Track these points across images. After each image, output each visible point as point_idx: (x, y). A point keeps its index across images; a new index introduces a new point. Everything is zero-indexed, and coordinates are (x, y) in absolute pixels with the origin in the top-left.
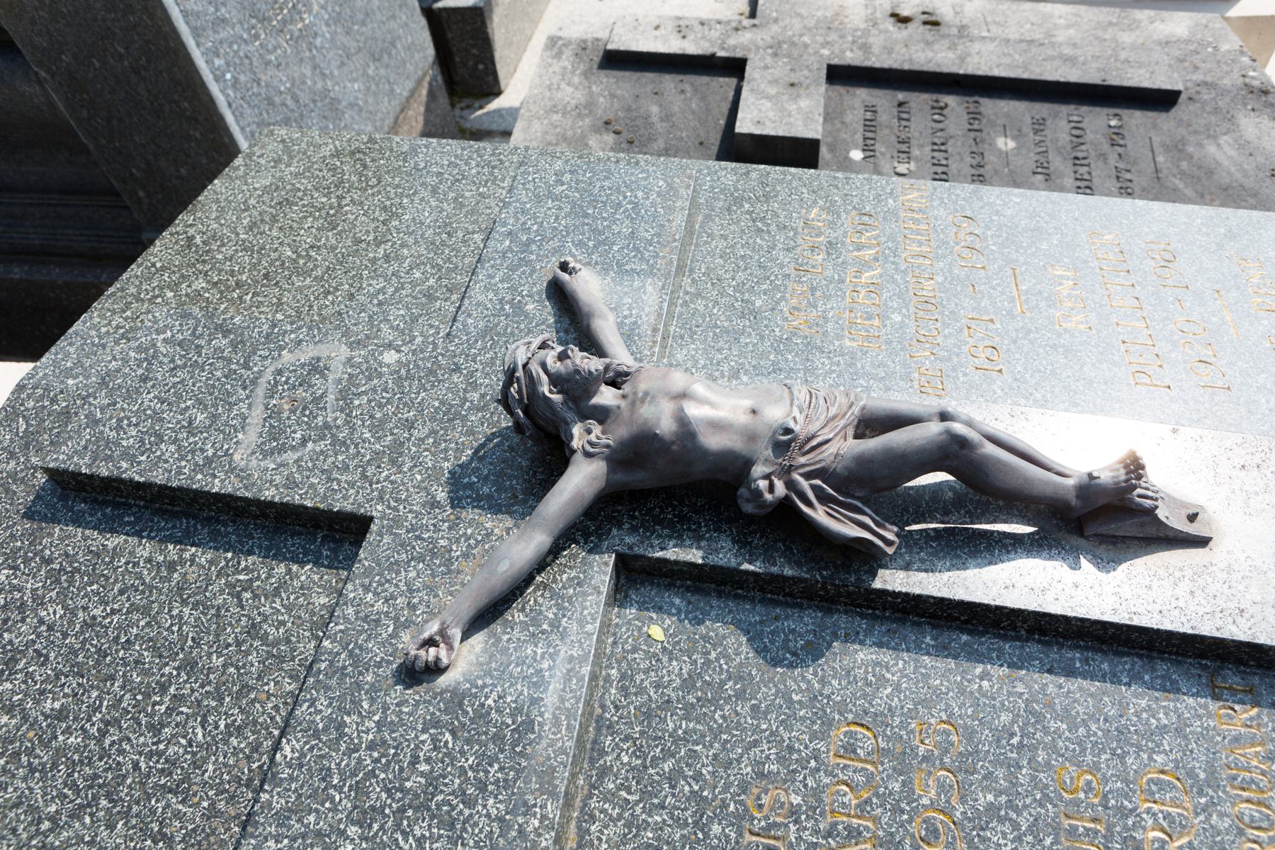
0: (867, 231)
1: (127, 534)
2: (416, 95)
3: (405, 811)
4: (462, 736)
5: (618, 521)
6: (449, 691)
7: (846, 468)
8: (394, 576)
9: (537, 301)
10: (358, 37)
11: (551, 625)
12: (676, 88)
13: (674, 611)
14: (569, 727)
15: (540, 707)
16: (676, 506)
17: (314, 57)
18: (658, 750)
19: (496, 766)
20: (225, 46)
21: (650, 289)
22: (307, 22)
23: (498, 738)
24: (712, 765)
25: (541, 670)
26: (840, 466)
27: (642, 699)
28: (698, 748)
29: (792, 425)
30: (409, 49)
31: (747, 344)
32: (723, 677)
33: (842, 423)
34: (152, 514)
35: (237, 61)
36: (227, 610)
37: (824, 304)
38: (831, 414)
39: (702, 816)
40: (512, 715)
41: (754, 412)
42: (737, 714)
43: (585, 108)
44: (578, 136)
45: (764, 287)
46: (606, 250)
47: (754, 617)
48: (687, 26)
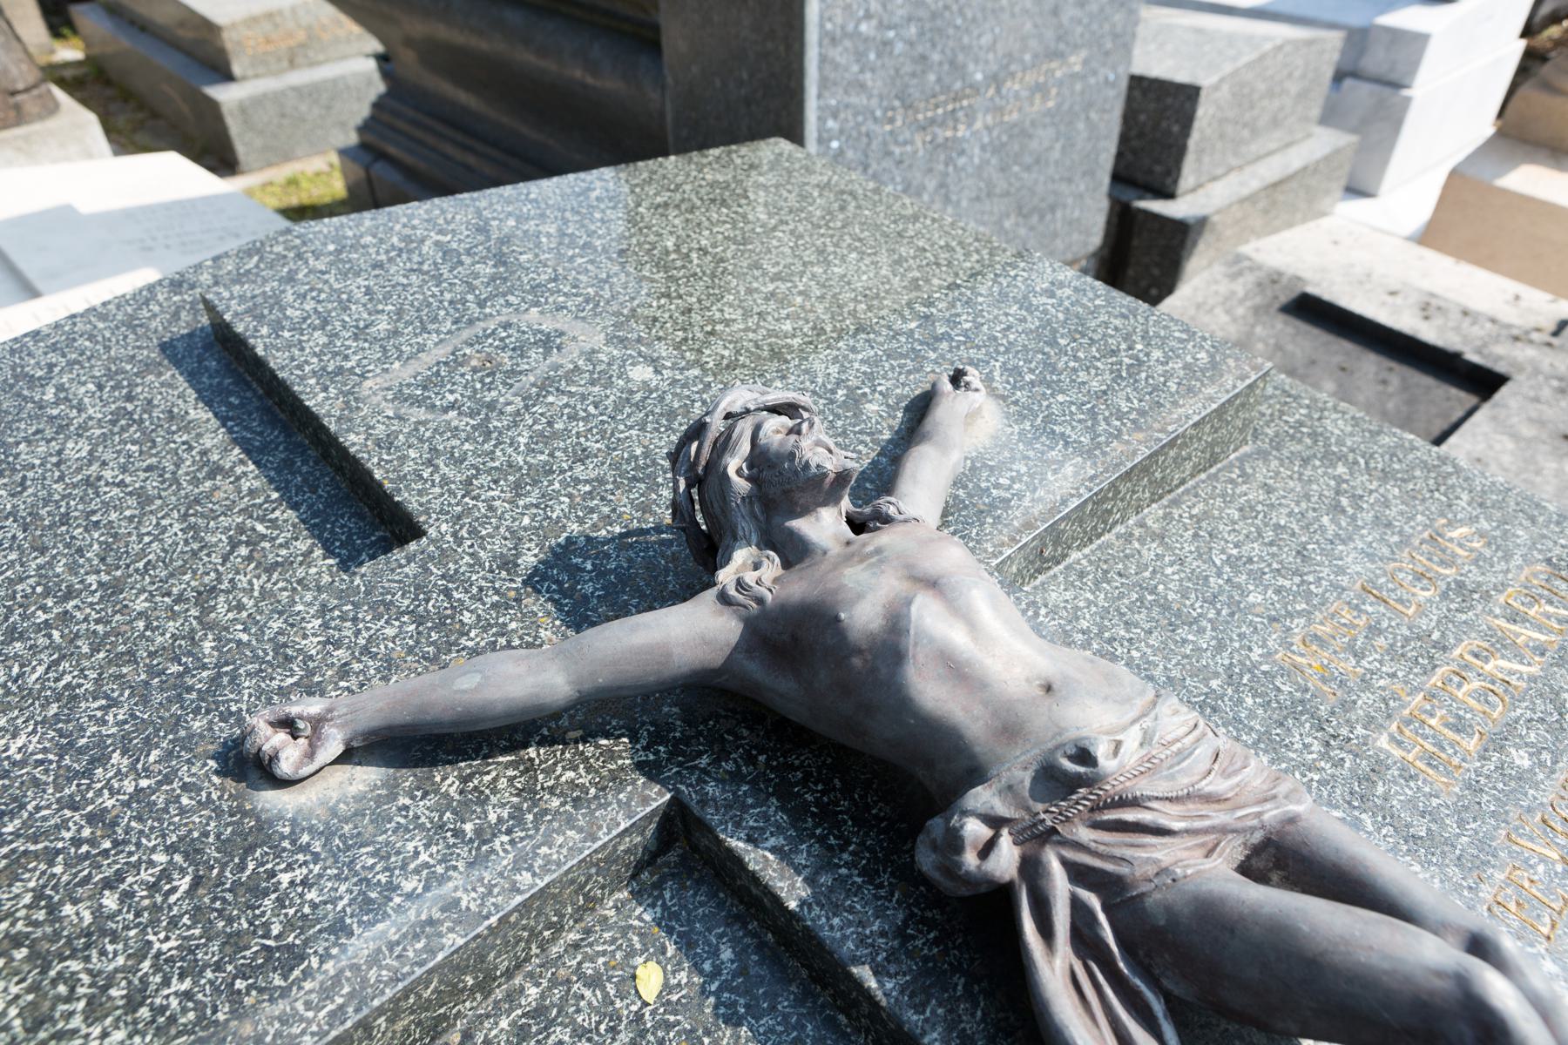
0: (1550, 602)
1: (216, 415)
4: (201, 898)
5: (723, 750)
6: (258, 819)
7: (1168, 909)
8: (368, 618)
9: (888, 406)
10: (1013, 180)
11: (478, 832)
12: (1377, 374)
13: (707, 966)
14: (337, 1015)
15: (335, 944)
16: (834, 789)
17: (946, 174)
19: (186, 984)
21: (1069, 469)
22: (960, 134)
25: (398, 887)
26: (1157, 896)
29: (1101, 751)
30: (1070, 223)
31: (1184, 641)
33: (1219, 817)
34: (257, 409)
35: (854, 134)
36: (209, 555)
37: (1381, 662)
38: (1208, 786)
40: (289, 925)
41: (1048, 688)
45: (1281, 582)
46: (1044, 394)
48: (1439, 308)
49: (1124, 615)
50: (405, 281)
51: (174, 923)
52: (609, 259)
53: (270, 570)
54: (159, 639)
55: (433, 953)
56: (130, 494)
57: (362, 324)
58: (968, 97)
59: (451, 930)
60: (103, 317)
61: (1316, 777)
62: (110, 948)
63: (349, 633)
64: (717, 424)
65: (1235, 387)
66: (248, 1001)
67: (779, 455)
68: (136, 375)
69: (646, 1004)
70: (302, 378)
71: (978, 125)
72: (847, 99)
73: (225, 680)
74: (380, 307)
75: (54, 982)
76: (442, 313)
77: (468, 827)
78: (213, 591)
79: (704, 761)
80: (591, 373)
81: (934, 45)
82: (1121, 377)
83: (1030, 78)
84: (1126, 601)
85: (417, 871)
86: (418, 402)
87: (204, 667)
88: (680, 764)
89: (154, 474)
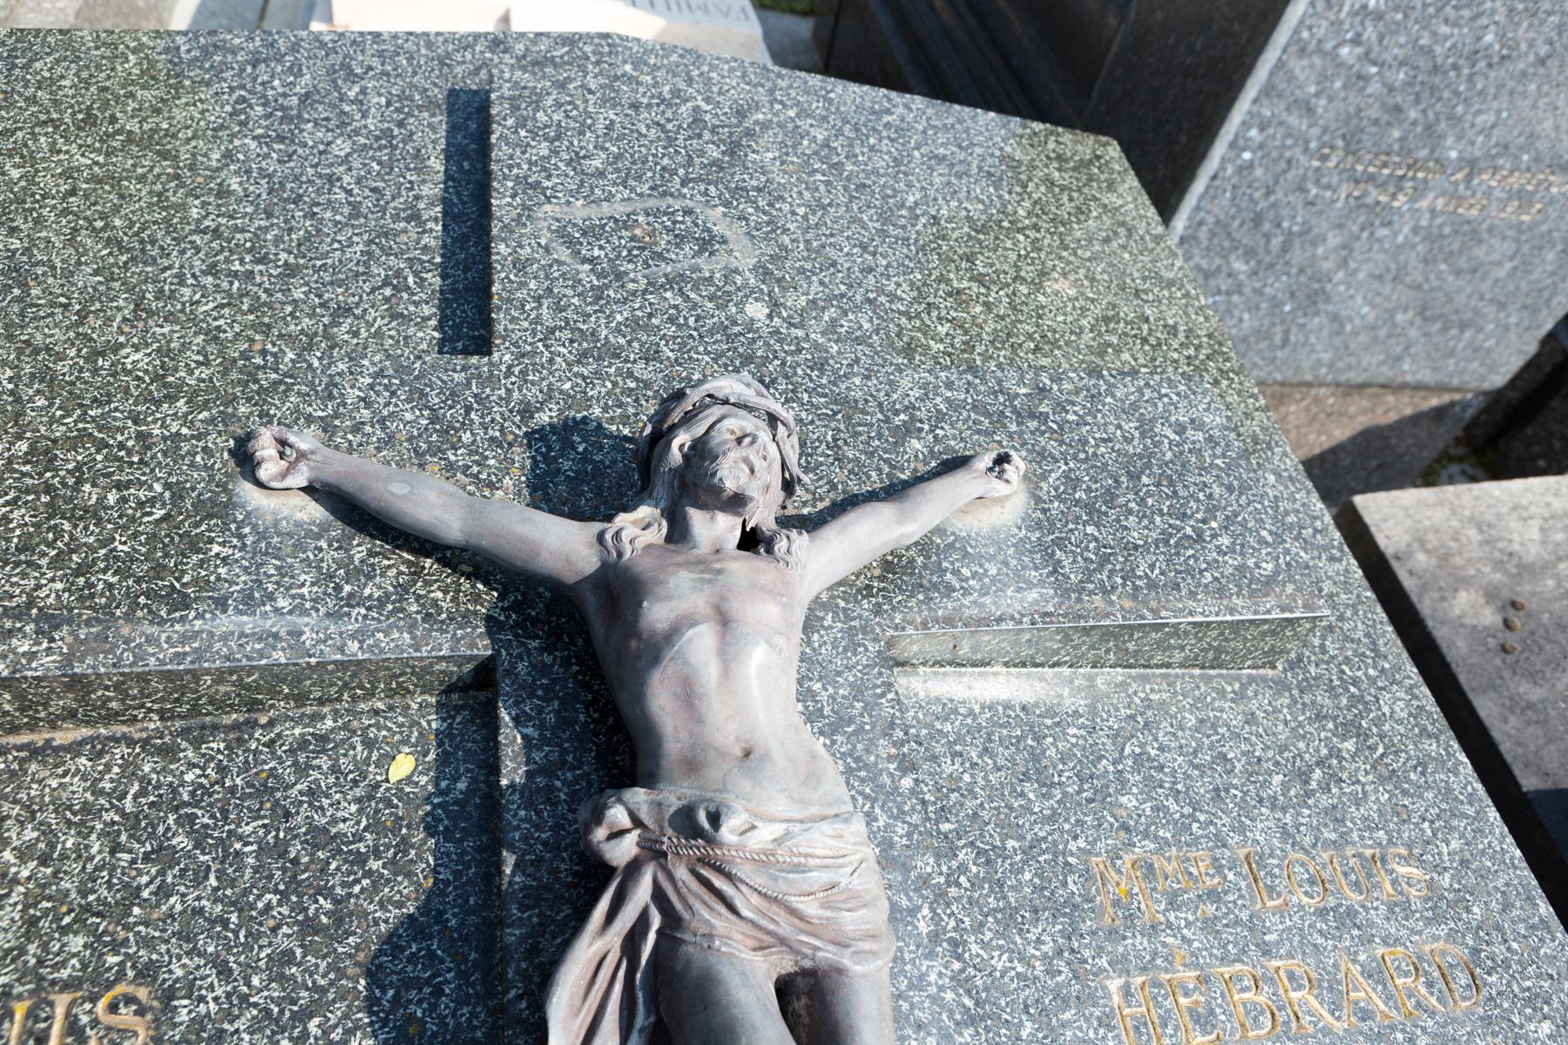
0: (1430, 985)
1: (446, 170)
2: (1422, 393)
3: (47, 492)
6: (230, 499)
7: (688, 962)
9: (931, 451)
10: (1432, 277)
11: (351, 595)
13: (443, 784)
14: (179, 657)
15: (211, 612)
17: (1358, 238)
18: (206, 820)
20: (1281, 131)
21: (1033, 595)
23: (159, 570)
24: (185, 911)
25: (275, 600)
26: (691, 949)
27: (288, 774)
28: (213, 881)
31: (1023, 795)
32: (338, 890)
33: (785, 926)
37: (1188, 924)
39: (98, 914)
41: (747, 754)
42: (274, 930)
43: (1519, 566)
44: (1463, 573)
46: (1078, 518)
47: (455, 915)
49: (991, 741)
50: (644, 131)
51: (136, 535)
52: (845, 188)
53: (393, 317)
54: (292, 327)
55: (262, 657)
56: (349, 203)
57: (583, 153)
58: (1428, 170)
59: (283, 649)
60: (429, 45)
61: (1020, 969)
62: (92, 527)
63: (381, 401)
64: (694, 396)
65: (1269, 612)
66: (139, 614)
67: (710, 451)
68: (418, 107)
69: (387, 780)
70: (505, 178)
71: (1424, 204)
72: (1284, 115)
73: (283, 388)
74: (608, 145)
75: (49, 529)
76: (649, 174)
77: (347, 588)
78: (347, 311)
79: (535, 644)
80: (719, 289)
81: (1417, 101)
82: (1166, 542)
83: (1515, 181)
84: (1005, 732)
85: (293, 597)
86: (570, 243)
87: (276, 371)
88: (516, 636)
89: (374, 196)
